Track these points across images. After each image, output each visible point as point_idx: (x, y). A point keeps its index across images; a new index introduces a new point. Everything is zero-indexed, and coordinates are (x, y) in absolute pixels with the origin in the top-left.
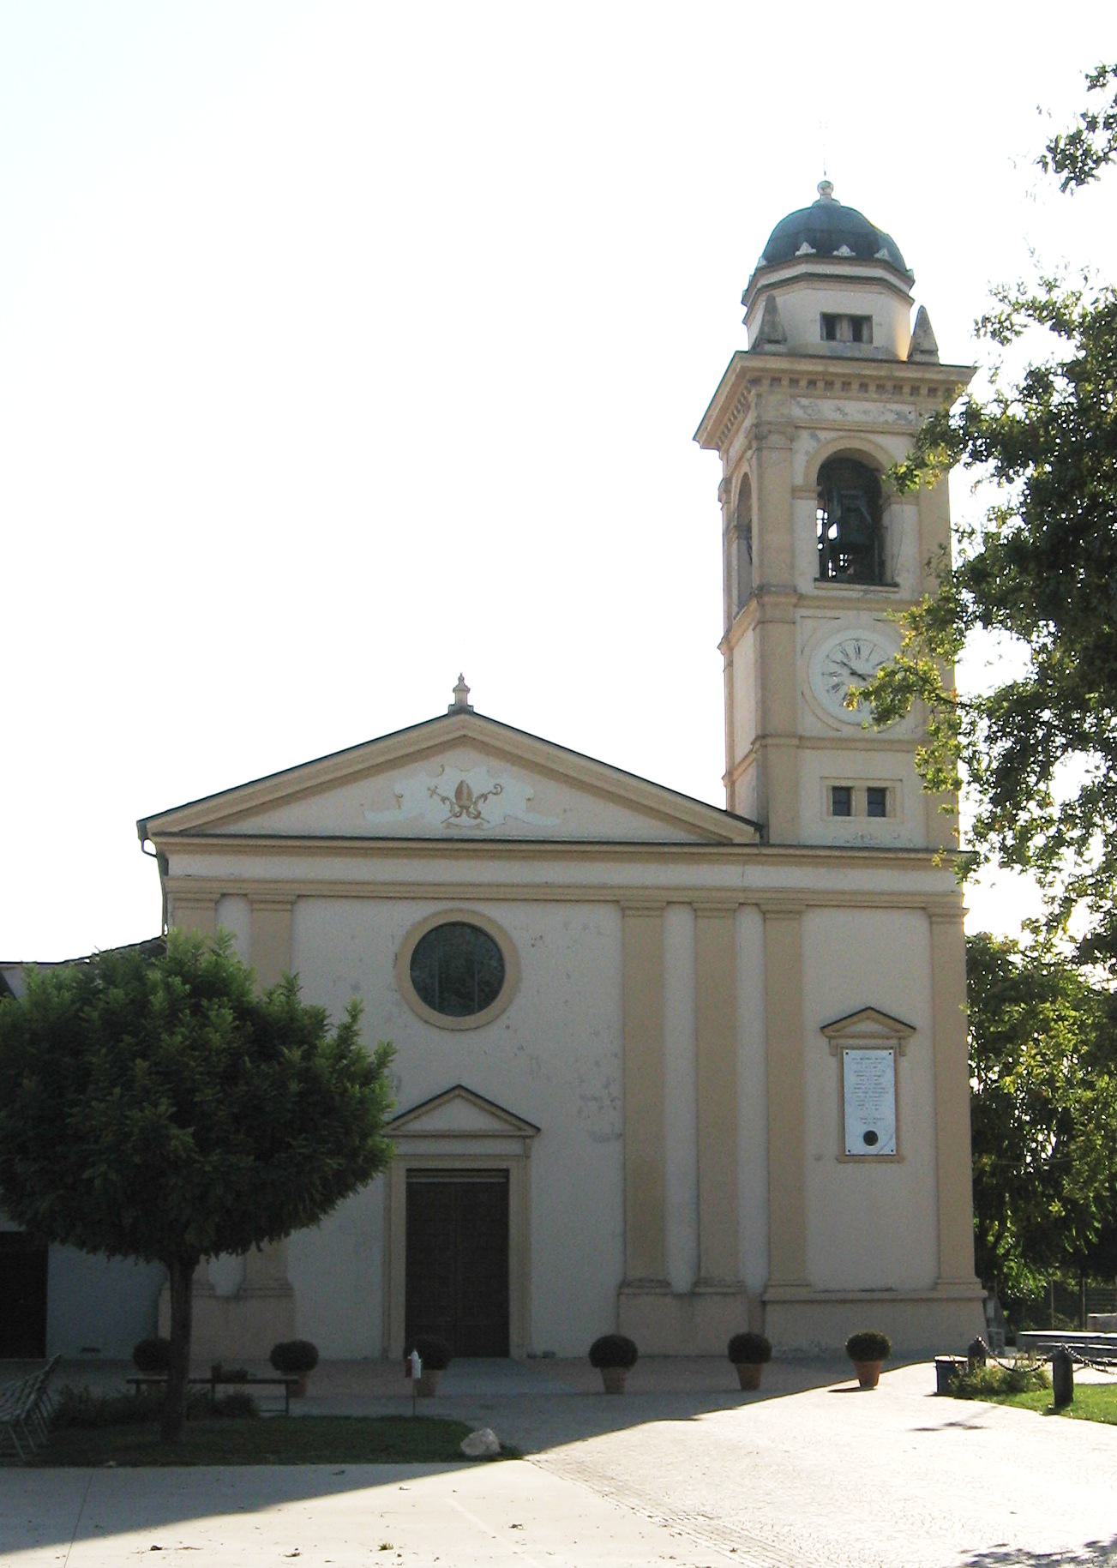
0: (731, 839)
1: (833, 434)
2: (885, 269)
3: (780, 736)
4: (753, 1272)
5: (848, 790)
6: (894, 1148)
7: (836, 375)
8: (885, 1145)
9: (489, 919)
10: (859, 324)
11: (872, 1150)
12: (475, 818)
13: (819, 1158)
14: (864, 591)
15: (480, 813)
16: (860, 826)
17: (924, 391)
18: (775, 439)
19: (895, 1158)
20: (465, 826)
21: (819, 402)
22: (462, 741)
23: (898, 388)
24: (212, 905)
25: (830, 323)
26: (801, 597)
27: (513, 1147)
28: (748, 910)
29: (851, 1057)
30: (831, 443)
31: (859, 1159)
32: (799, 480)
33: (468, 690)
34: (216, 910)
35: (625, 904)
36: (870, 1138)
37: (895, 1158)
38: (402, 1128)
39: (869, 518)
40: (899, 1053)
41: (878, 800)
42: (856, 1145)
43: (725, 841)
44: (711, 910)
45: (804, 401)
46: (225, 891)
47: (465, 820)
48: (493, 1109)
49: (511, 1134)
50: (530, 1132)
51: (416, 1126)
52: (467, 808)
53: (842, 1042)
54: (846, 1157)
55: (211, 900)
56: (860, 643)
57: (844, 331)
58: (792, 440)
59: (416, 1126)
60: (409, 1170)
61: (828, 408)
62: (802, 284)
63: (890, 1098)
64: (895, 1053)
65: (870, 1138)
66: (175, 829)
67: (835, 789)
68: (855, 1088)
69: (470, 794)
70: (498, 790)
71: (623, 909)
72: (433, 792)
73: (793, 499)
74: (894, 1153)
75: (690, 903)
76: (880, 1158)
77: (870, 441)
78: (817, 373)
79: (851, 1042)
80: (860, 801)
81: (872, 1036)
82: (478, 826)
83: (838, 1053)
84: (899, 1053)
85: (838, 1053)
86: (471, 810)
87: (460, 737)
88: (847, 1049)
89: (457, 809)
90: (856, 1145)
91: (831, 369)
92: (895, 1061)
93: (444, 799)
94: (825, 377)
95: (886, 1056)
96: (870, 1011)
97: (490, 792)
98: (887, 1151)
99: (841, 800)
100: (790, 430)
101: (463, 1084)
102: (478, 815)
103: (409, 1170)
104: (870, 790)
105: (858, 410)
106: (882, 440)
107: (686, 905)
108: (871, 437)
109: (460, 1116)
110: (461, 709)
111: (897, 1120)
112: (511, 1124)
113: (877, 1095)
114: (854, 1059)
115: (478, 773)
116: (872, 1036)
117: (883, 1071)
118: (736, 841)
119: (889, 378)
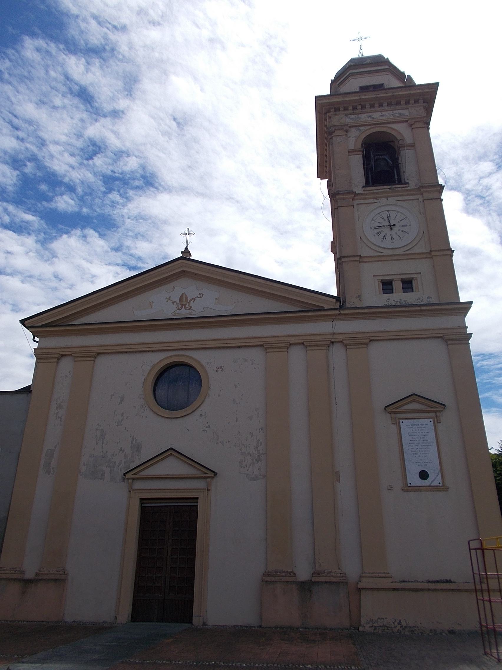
8: (434, 479)
19: (442, 488)
31: (418, 489)
42: (416, 481)
52: (185, 305)
54: (407, 488)
65: (424, 475)
70: (201, 295)
89: (180, 306)
97: (197, 297)
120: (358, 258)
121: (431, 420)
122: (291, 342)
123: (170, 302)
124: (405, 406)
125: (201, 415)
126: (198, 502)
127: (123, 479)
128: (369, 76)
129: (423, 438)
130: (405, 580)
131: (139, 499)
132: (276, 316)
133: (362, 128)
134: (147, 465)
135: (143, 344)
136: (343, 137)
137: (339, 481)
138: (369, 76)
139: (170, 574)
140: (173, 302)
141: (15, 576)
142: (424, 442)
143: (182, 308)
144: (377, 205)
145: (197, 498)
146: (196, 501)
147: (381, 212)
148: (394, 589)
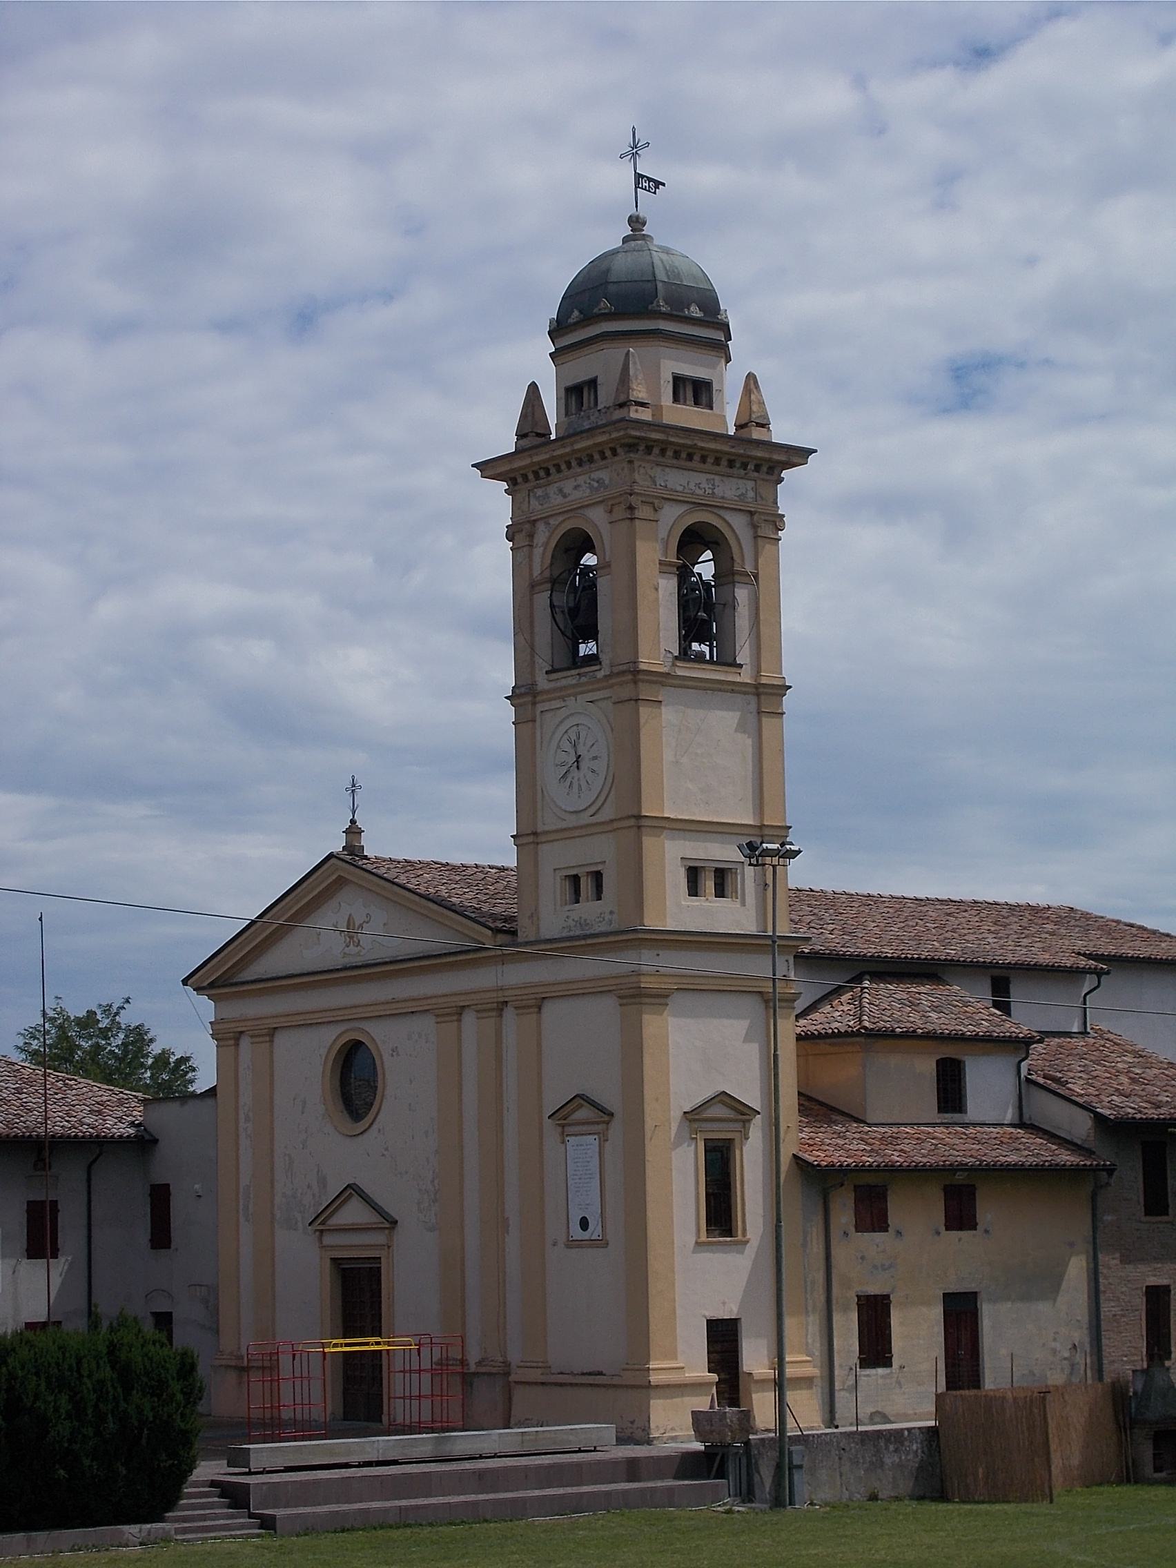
6: (574, 1238)
8: (594, 1231)
11: (586, 1235)
13: (554, 1245)
19: (601, 1243)
24: (267, 1039)
27: (379, 1238)
28: (467, 1010)
33: (361, 832)
34: (272, 1041)
36: (584, 1224)
38: (329, 1222)
40: (603, 1139)
42: (577, 1233)
44: (488, 1003)
54: (572, 1244)
55: (492, 1010)
65: (584, 1224)
66: (205, 984)
68: (575, 1170)
74: (600, 1238)
79: (576, 1129)
82: (358, 954)
84: (603, 1139)
94: (543, 466)
96: (1088, 997)
102: (358, 944)
110: (353, 850)
120: (531, 839)
121: (596, 1137)
124: (576, 1113)
125: (379, 1130)
126: (380, 1263)
127: (317, 1233)
128: (586, 353)
129: (577, 1166)
130: (564, 1371)
131: (329, 1260)
132: (438, 961)
133: (552, 521)
134: (331, 1209)
135: (391, 962)
136: (525, 549)
137: (508, 1233)
138: (586, 353)
139: (372, 1361)
141: (233, 1363)
142: (589, 1176)
144: (562, 713)
145: (380, 1258)
146: (378, 1260)
147: (560, 741)
148: (543, 1384)
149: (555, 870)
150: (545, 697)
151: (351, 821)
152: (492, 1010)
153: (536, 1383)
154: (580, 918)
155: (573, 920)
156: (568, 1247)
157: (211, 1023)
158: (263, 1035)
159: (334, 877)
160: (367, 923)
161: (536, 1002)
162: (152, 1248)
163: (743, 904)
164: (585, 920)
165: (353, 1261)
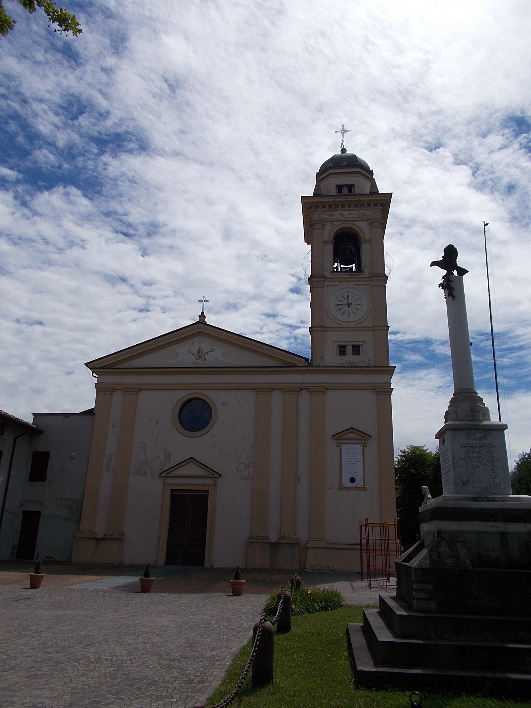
0: (297, 365)
1: (339, 223)
2: (360, 168)
3: (318, 327)
4: (303, 535)
5: (345, 347)
7: (339, 202)
8: (359, 483)
9: (208, 397)
10: (350, 187)
12: (204, 360)
13: (331, 488)
14: (350, 275)
15: (205, 358)
16: (350, 358)
17: (372, 205)
18: (316, 226)
19: (364, 488)
20: (200, 363)
21: (334, 213)
22: (199, 333)
23: (362, 205)
25: (340, 188)
26: (326, 278)
28: (304, 391)
29: (344, 448)
30: (338, 226)
31: (348, 488)
32: (326, 239)
35: (256, 389)
36: (352, 480)
37: (364, 488)
39: (354, 251)
40: (365, 446)
41: (356, 349)
42: (347, 483)
43: (295, 365)
45: (329, 213)
46: (141, 388)
47: (200, 361)
48: (205, 467)
49: (211, 476)
50: (217, 476)
51: (173, 473)
53: (341, 441)
54: (342, 488)
55: (296, 391)
56: (349, 293)
57: (345, 191)
58: (323, 226)
59: (173, 473)
60: (171, 490)
61: (337, 215)
62: (330, 176)
63: (361, 463)
64: (363, 446)
65: (352, 480)
66: (99, 367)
67: (340, 346)
69: (202, 352)
71: (256, 391)
72: (190, 351)
73: (323, 245)
75: (254, 389)
76: (357, 489)
77: (353, 224)
78: (331, 202)
80: (349, 350)
81: (354, 439)
83: (339, 446)
84: (365, 446)
85: (339, 446)
86: (203, 357)
87: (198, 332)
88: (343, 444)
90: (347, 483)
91: (336, 200)
92: (363, 449)
93: (193, 354)
94: (335, 203)
95: (359, 448)
97: (210, 351)
98: (359, 486)
99: (342, 350)
100: (323, 222)
101: (193, 457)
102: (205, 359)
103: (171, 490)
104: (353, 346)
105: (347, 214)
106: (360, 224)
107: (371, 391)
108: (355, 223)
109: (191, 469)
111: (364, 473)
112: (358, 435)
113: (355, 463)
114: (346, 448)
115: (205, 344)
116: (354, 439)
117: (358, 453)
118: (298, 365)
119: (358, 201)
122: (114, 388)
123: (191, 354)
125: (211, 436)
126: (208, 493)
136: (320, 230)
137: (299, 483)
140: (193, 354)
143: (199, 359)
149: (334, 342)
150: (330, 280)
151: (202, 313)
152: (296, 391)
153: (324, 548)
154: (350, 361)
155: (346, 361)
156: (339, 489)
157: (95, 384)
158: (134, 391)
159: (198, 331)
160: (212, 351)
161: (325, 389)
162: (30, 480)
163: (395, 367)
164: (353, 362)
165: (184, 491)
